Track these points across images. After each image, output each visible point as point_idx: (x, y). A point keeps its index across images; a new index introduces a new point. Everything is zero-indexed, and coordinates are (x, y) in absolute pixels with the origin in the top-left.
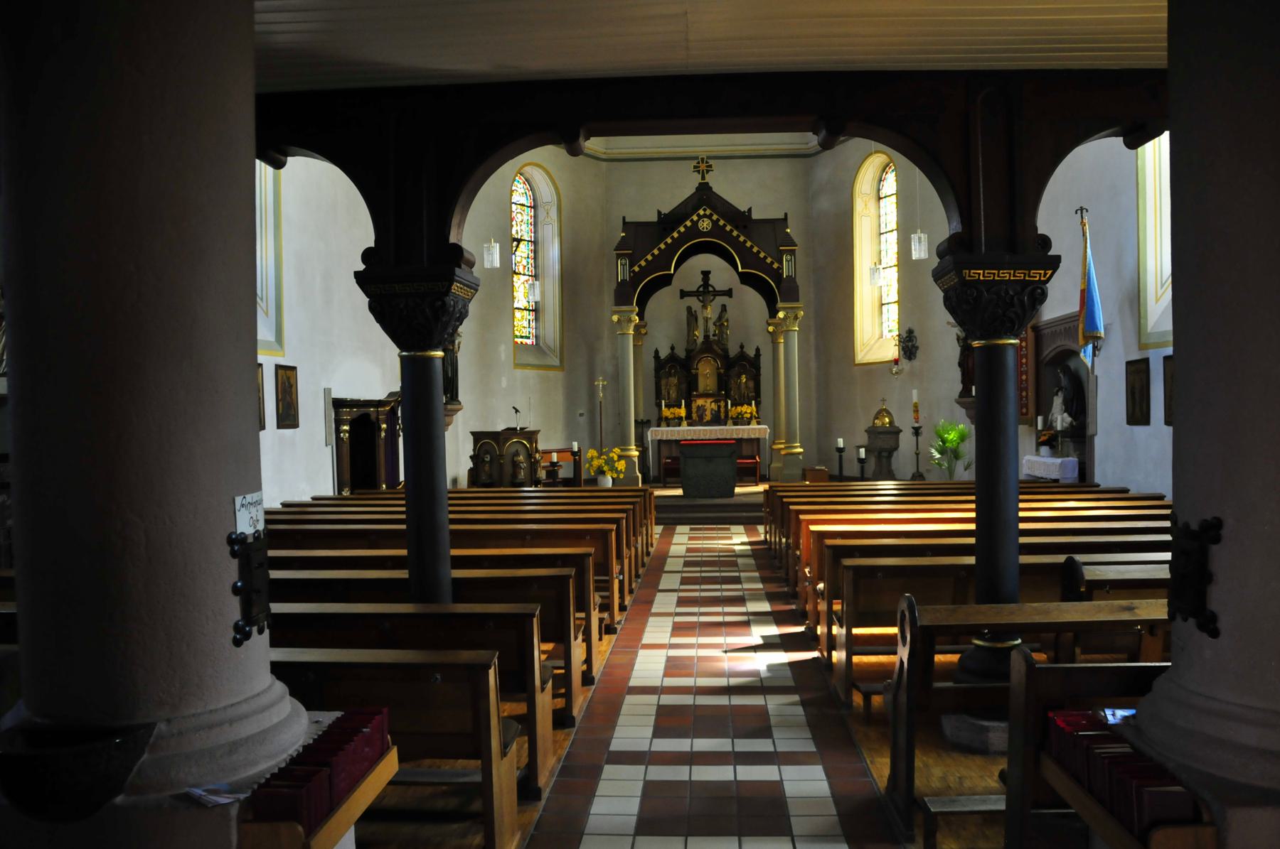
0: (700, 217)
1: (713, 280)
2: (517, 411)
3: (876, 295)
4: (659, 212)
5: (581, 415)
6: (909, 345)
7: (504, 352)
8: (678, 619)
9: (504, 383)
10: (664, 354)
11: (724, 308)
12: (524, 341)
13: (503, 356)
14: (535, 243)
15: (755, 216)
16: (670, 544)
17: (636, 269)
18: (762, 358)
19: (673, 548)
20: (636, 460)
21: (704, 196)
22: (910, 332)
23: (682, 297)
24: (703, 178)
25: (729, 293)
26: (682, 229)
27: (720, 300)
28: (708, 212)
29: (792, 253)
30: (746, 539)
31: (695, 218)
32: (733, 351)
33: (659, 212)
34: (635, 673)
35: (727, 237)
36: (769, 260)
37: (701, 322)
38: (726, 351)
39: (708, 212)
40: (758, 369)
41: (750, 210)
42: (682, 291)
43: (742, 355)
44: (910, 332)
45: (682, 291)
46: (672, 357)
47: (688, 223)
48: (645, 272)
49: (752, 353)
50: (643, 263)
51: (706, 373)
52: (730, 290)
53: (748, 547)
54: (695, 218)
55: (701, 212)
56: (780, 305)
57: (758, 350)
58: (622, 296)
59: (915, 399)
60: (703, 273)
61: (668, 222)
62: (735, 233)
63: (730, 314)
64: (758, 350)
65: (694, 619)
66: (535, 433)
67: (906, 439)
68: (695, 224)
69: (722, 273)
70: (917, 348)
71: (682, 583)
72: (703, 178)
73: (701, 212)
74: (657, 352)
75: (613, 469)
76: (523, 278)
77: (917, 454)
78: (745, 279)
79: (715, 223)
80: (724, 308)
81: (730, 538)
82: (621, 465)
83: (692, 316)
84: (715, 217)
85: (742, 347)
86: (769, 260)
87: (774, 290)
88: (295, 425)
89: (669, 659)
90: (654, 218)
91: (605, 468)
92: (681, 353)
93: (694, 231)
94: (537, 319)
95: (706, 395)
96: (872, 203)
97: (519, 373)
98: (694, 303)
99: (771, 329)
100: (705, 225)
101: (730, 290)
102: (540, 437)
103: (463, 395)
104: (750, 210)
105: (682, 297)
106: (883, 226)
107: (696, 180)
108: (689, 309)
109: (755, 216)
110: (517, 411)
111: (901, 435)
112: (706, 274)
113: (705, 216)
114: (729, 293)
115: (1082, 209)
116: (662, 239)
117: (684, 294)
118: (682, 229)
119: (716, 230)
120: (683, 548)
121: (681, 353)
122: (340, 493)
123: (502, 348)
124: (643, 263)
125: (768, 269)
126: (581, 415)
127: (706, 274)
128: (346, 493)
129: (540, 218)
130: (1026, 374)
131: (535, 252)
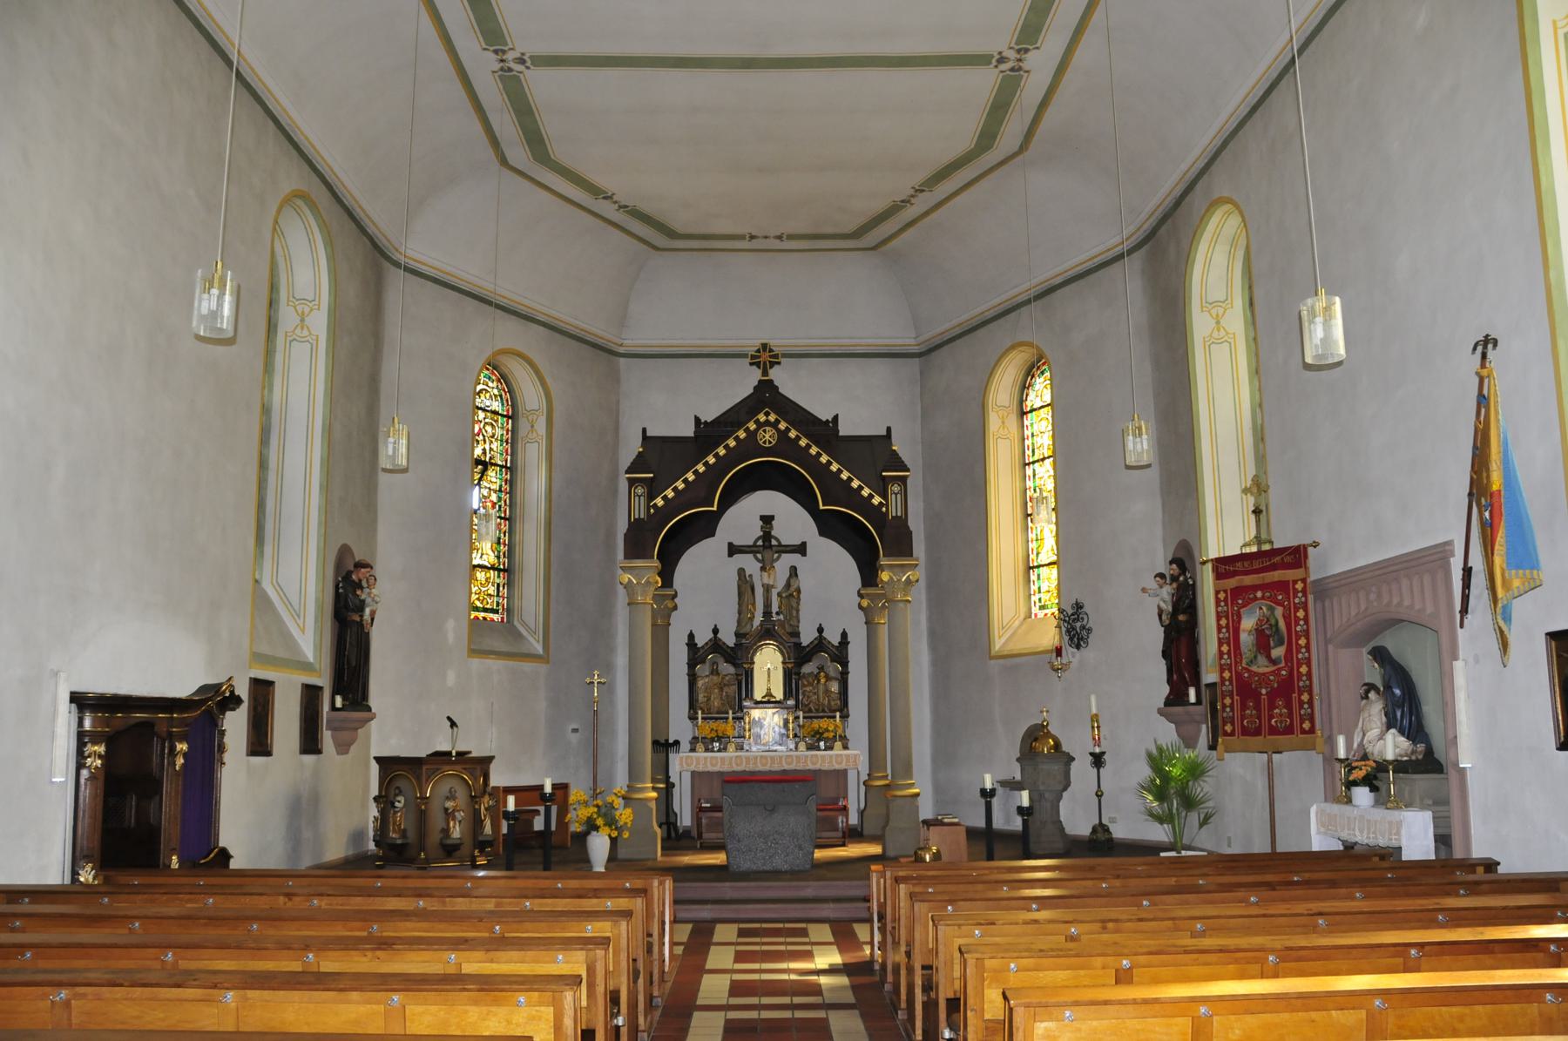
0: (759, 425)
1: (778, 530)
2: (453, 724)
3: (1021, 554)
4: (697, 420)
5: (575, 731)
6: (1075, 626)
7: (454, 631)
8: (733, 1015)
9: (451, 678)
10: (702, 639)
11: (794, 571)
13: (451, 637)
14: (511, 469)
15: (844, 430)
16: (701, 970)
17: (659, 502)
19: (707, 980)
20: (653, 805)
21: (766, 396)
22: (1078, 606)
23: (731, 554)
24: (765, 373)
25: (801, 549)
26: (732, 443)
27: (787, 560)
28: (772, 418)
29: (903, 480)
30: (836, 958)
31: (752, 426)
32: (807, 637)
33: (697, 420)
34: (701, 994)
35: (802, 456)
36: (866, 492)
37: (759, 591)
38: (797, 635)
39: (772, 418)
40: (845, 664)
41: (836, 418)
42: (730, 545)
43: (820, 644)
44: (1078, 606)
45: (730, 545)
46: (716, 645)
47: (742, 434)
48: (672, 507)
49: (835, 639)
50: (670, 494)
51: (768, 664)
52: (804, 544)
53: (843, 980)
54: (752, 426)
55: (762, 418)
56: (884, 561)
57: (844, 635)
58: (637, 543)
59: (1094, 711)
60: (763, 518)
61: (708, 434)
62: (814, 450)
63: (805, 581)
64: (844, 635)
65: (757, 948)
66: (488, 760)
67: (1081, 770)
68: (752, 435)
69: (793, 521)
70: (1089, 630)
71: (736, 961)
72: (765, 373)
73: (762, 418)
74: (691, 636)
75: (611, 822)
77: (1099, 795)
78: (829, 526)
79: (783, 435)
80: (794, 571)
81: (808, 955)
82: (625, 815)
83: (745, 585)
84: (783, 426)
85: (820, 630)
86: (866, 492)
87: (870, 540)
89: (733, 982)
90: (688, 431)
91: (600, 822)
92: (729, 639)
93: (750, 446)
95: (768, 701)
96: (1013, 420)
97: (476, 663)
98: (750, 563)
99: (865, 603)
100: (767, 437)
101: (804, 544)
102: (493, 767)
103: (377, 696)
104: (836, 418)
105: (731, 554)
106: (1029, 453)
107: (755, 376)
108: (741, 572)
109: (844, 430)
110: (453, 724)
111: (1074, 766)
112: (767, 520)
113: (767, 423)
114: (801, 549)
115: (1488, 342)
116: (700, 457)
117: (733, 550)
118: (732, 443)
119: (785, 445)
120: (723, 982)
121: (729, 639)
122: (75, 873)
123: (450, 624)
124: (670, 494)
125: (864, 505)
126: (575, 731)
127: (767, 520)
128: (87, 875)
130: (1308, 662)
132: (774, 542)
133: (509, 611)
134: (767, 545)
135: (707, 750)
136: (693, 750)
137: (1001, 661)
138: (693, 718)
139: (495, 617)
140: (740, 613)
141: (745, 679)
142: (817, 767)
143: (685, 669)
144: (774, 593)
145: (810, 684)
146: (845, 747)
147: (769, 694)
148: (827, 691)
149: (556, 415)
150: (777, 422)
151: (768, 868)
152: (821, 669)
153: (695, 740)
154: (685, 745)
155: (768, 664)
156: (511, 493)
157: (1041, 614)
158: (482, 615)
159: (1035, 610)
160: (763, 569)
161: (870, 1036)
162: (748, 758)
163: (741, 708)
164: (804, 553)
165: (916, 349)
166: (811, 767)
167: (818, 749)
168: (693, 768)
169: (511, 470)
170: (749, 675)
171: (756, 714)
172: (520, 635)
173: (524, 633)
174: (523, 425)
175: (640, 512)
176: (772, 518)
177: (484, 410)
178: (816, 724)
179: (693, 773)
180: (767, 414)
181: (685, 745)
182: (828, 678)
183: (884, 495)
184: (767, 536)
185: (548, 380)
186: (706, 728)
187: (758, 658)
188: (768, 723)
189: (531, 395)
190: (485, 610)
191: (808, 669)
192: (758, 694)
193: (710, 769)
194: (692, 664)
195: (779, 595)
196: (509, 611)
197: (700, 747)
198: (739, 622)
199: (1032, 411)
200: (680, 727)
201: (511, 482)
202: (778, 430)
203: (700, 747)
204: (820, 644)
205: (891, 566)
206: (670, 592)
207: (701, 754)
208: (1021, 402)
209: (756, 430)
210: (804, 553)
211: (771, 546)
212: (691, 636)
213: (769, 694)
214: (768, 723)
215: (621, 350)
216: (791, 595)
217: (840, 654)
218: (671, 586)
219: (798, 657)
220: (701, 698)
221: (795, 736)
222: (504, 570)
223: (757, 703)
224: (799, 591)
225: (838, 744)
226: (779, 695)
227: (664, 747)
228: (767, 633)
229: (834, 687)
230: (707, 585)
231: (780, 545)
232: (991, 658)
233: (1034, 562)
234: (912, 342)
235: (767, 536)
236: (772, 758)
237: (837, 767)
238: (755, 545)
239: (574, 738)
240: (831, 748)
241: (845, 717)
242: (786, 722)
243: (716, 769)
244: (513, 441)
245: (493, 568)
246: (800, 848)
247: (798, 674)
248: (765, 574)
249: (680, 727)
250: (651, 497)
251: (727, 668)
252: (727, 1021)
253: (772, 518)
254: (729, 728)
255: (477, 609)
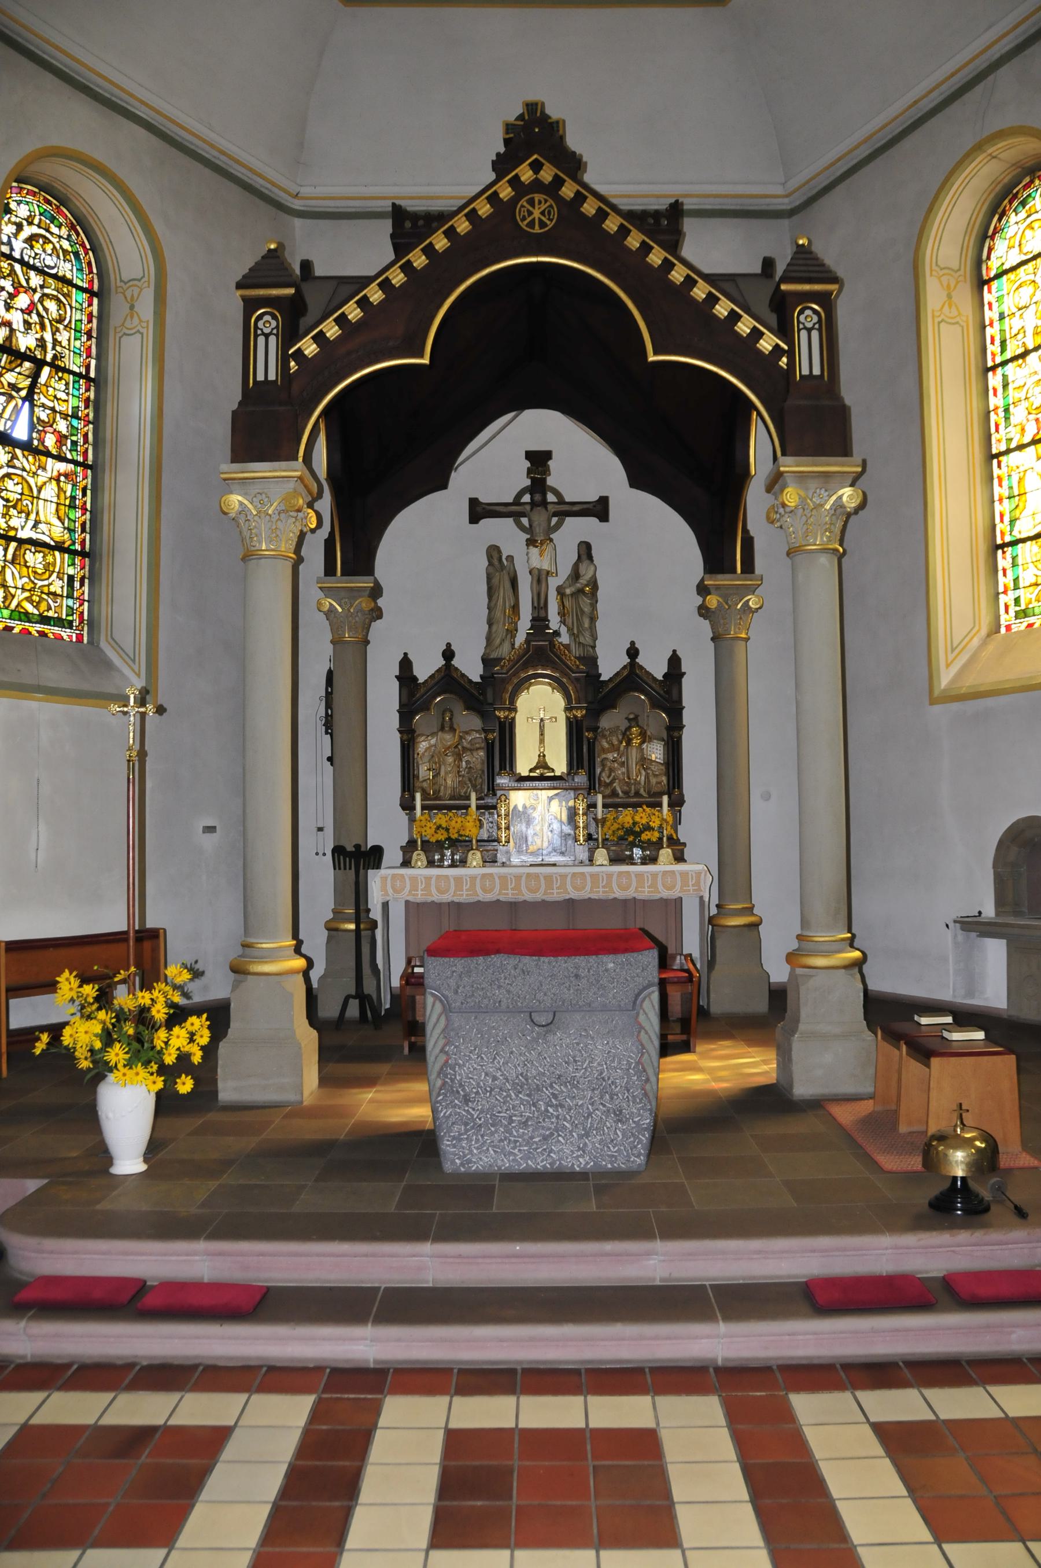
5: (210, 829)
10: (424, 670)
11: (585, 551)
12: (51, 630)
18: (688, 685)
25: (600, 509)
29: (826, 301)
32: (610, 664)
36: (744, 327)
38: (592, 661)
39: (547, 175)
40: (675, 711)
42: (474, 503)
43: (633, 676)
45: (474, 503)
46: (448, 678)
49: (658, 669)
51: (541, 716)
52: (604, 501)
55: (526, 174)
57: (674, 661)
63: (606, 572)
64: (674, 661)
69: (585, 460)
74: (406, 664)
76: (56, 467)
80: (585, 551)
83: (499, 569)
86: (744, 327)
88: (204, 832)
92: (471, 667)
94: (93, 578)
95: (541, 776)
98: (505, 534)
101: (604, 501)
106: (993, 349)
108: (493, 552)
113: (537, 186)
114: (600, 509)
117: (478, 511)
121: (471, 667)
126: (210, 829)
129: (114, 321)
131: (98, 405)
132: (551, 498)
133: (92, 624)
134: (538, 501)
135: (431, 863)
136: (406, 863)
137: (955, 706)
138: (407, 806)
139: (65, 634)
140: (490, 623)
141: (501, 748)
142: (630, 893)
143: (394, 720)
144: (554, 583)
145: (615, 748)
146: (679, 858)
147: (542, 764)
148: (644, 761)
149: (172, 287)
150: (558, 182)
151: (541, 1164)
152: (634, 721)
153: (410, 847)
154: (392, 855)
155: (541, 716)
156: (97, 423)
157: (1020, 626)
158: (34, 628)
159: (1005, 619)
160: (531, 542)
161: (775, 1556)
162: (503, 878)
163: (492, 789)
164: (604, 517)
165: (785, 204)
166: (619, 894)
167: (630, 860)
168: (406, 895)
169: (97, 382)
170: (506, 732)
171: (519, 798)
172: (109, 665)
173: (117, 661)
174: (118, 306)
175: (267, 367)
176: (547, 455)
177: (40, 272)
178: (627, 817)
179: (407, 903)
180: (536, 167)
181: (392, 855)
182: (645, 737)
183: (784, 330)
184: (538, 485)
185: (159, 227)
186: (429, 827)
187: (524, 701)
188: (540, 818)
189: (129, 253)
190: (44, 620)
191: (609, 721)
192: (523, 767)
193: (436, 897)
194: (406, 713)
195: (560, 591)
196: (91, 624)
197: (419, 857)
198: (489, 639)
199: (998, 276)
200: (387, 825)
201: (98, 405)
202: (560, 200)
203: (419, 857)
204: (633, 676)
205: (802, 477)
206: (364, 583)
207: (420, 870)
208: (979, 263)
209: (514, 201)
210: (604, 517)
211: (544, 503)
212: (406, 664)
213: (542, 764)
214: (540, 818)
215: (297, 205)
216: (582, 592)
217: (668, 693)
218: (368, 569)
219: (595, 699)
220: (424, 771)
221: (589, 837)
222: (83, 554)
223: (522, 779)
224: (594, 584)
225: (666, 853)
226: (559, 765)
227: (357, 859)
228: (541, 655)
229: (656, 752)
230: (435, 580)
231: (561, 501)
232: (933, 701)
233: (1004, 532)
234: (779, 190)
235: (538, 485)
236: (548, 878)
237: (665, 894)
238: (517, 501)
239: (209, 841)
240: (653, 860)
241: (677, 803)
242: (573, 813)
243: (446, 898)
244: (101, 335)
245: (59, 547)
246: (619, 1116)
247: (595, 729)
248: (534, 551)
249: (387, 825)
250: (290, 334)
251: (469, 722)
252: (456, 1441)
253: (547, 455)
254: (467, 824)
255: (27, 617)
